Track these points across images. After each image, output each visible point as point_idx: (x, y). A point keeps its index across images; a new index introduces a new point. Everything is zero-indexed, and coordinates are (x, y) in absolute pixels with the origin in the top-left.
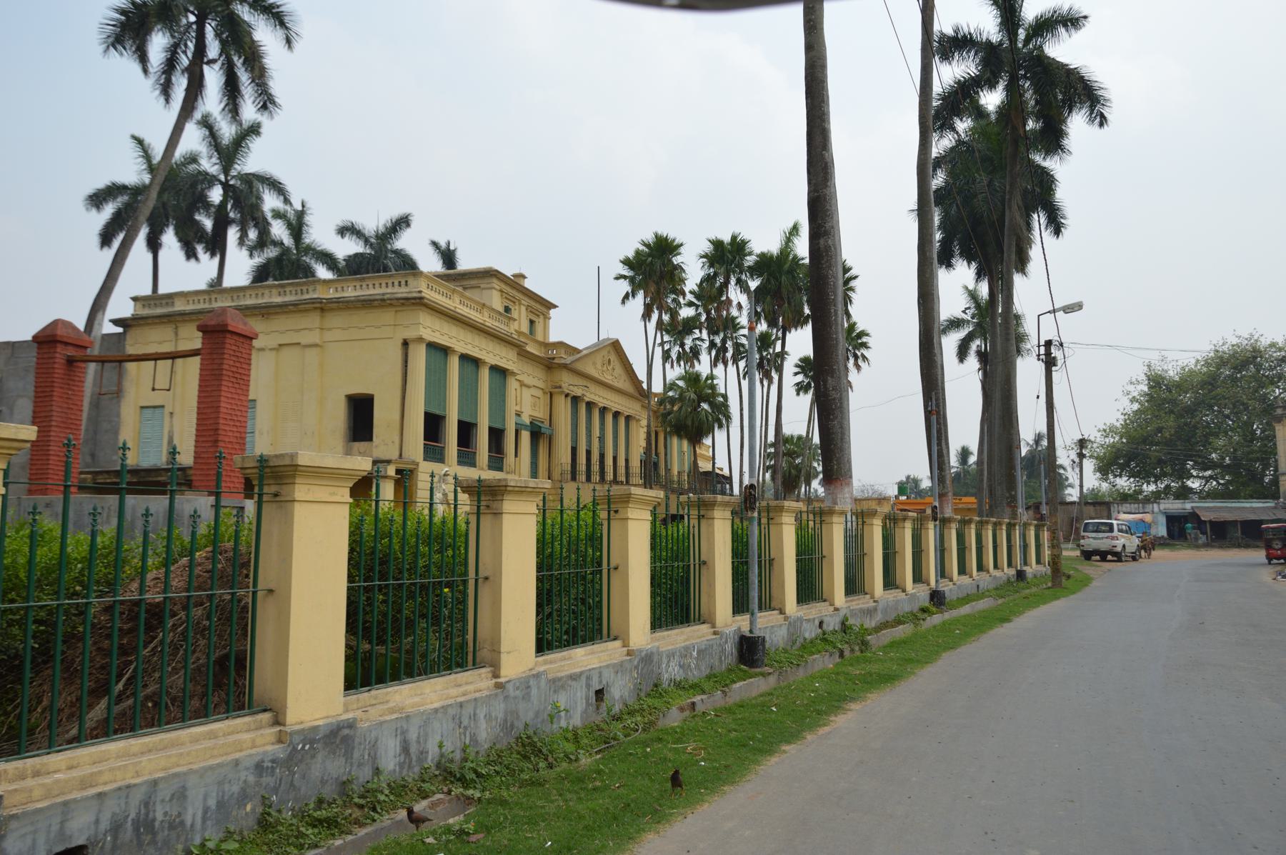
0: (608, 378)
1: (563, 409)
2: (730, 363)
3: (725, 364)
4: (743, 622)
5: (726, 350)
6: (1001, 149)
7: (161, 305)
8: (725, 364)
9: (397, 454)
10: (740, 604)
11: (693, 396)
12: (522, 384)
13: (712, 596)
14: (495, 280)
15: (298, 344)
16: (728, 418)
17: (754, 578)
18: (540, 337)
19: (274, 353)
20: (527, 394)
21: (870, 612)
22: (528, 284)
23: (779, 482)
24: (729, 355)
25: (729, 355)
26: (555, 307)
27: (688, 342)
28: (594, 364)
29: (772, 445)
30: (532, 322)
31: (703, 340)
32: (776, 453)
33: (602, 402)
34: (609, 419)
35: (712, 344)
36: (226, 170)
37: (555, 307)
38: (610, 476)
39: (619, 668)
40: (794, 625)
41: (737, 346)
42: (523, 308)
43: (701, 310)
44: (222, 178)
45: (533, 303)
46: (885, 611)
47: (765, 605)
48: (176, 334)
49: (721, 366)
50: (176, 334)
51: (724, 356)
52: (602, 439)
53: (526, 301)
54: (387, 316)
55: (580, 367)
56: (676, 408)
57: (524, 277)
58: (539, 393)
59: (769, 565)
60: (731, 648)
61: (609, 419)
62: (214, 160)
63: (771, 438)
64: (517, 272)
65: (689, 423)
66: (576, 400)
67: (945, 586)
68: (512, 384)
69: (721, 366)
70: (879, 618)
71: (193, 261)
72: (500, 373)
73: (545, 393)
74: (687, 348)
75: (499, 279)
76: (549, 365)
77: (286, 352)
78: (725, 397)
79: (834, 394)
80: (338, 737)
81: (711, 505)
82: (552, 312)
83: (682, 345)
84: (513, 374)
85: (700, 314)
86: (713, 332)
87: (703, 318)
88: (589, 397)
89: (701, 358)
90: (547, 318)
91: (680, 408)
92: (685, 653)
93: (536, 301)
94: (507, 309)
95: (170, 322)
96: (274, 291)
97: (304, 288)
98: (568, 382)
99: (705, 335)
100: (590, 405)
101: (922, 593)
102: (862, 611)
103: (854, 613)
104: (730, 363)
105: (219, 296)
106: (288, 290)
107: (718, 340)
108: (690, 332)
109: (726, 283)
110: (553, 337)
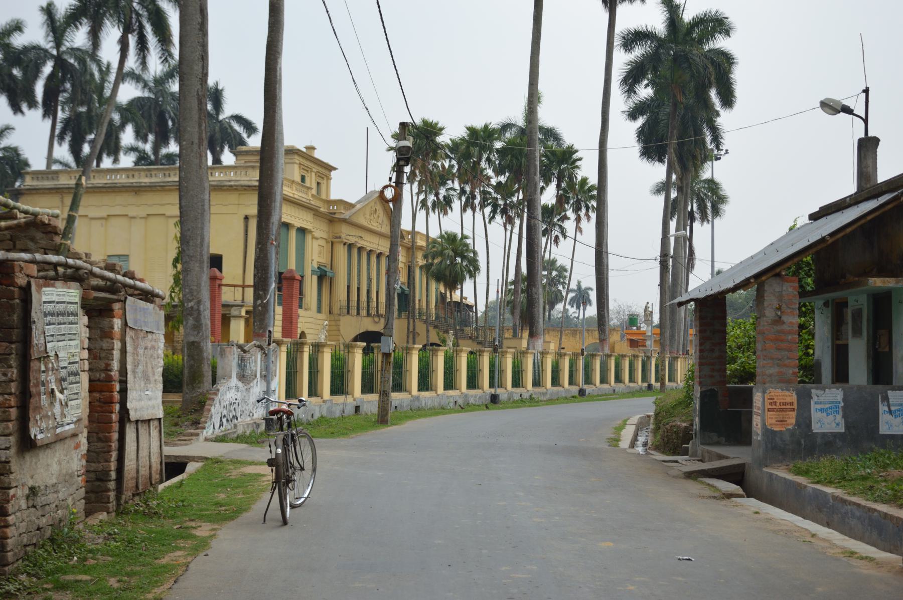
0: (374, 226)
1: (341, 253)
2: (478, 209)
3: (474, 210)
4: (493, 391)
5: (474, 197)
6: (682, 87)
7: (48, 179)
8: (474, 210)
9: (241, 298)
10: (492, 385)
11: (451, 253)
12: (314, 238)
13: (483, 381)
14: (296, 157)
15: (164, 214)
16: (477, 268)
17: (496, 376)
18: (324, 197)
19: (143, 220)
20: (316, 243)
21: (544, 394)
22: (317, 154)
23: (518, 316)
24: (477, 201)
25: (477, 201)
26: (335, 169)
27: (442, 192)
28: (365, 214)
29: (513, 283)
30: (318, 184)
31: (455, 190)
32: (515, 291)
33: (369, 246)
34: (374, 258)
35: (463, 192)
36: (58, 43)
37: (335, 169)
38: (374, 312)
39: (460, 397)
40: (510, 395)
41: (484, 193)
42: (313, 174)
43: (454, 162)
44: (55, 52)
45: (320, 169)
46: (551, 394)
47: (500, 386)
48: (62, 202)
49: (469, 211)
50: (62, 202)
51: (473, 203)
52: (369, 280)
53: (316, 168)
54: (233, 197)
55: (355, 220)
56: (436, 261)
57: (314, 148)
58: (323, 243)
59: (502, 372)
60: (488, 398)
61: (374, 258)
62: (50, 38)
63: (511, 277)
64: (309, 144)
65: (448, 273)
66: (350, 246)
67: (589, 389)
68: (309, 238)
69: (469, 211)
70: (548, 396)
71: (19, 115)
72: (302, 231)
73: (327, 242)
74: (441, 197)
75: (299, 155)
76: (331, 219)
77: (153, 221)
78: (475, 253)
79: (535, 296)
80: (418, 398)
81: (483, 351)
82: (333, 173)
83: (437, 195)
84: (311, 232)
85: (453, 166)
86: (462, 181)
87: (455, 170)
88: (361, 243)
89: (453, 205)
90: (329, 178)
91: (441, 262)
92: (475, 396)
93: (322, 166)
94: (303, 179)
95: (57, 192)
96: (143, 173)
97: (167, 173)
98: (347, 234)
99: (457, 185)
100: (360, 249)
101: (575, 389)
102: (540, 393)
103: (535, 393)
104: (478, 209)
105: (97, 175)
106: (153, 173)
107: (468, 189)
108: (444, 183)
109: (480, 159)
110: (334, 196)
